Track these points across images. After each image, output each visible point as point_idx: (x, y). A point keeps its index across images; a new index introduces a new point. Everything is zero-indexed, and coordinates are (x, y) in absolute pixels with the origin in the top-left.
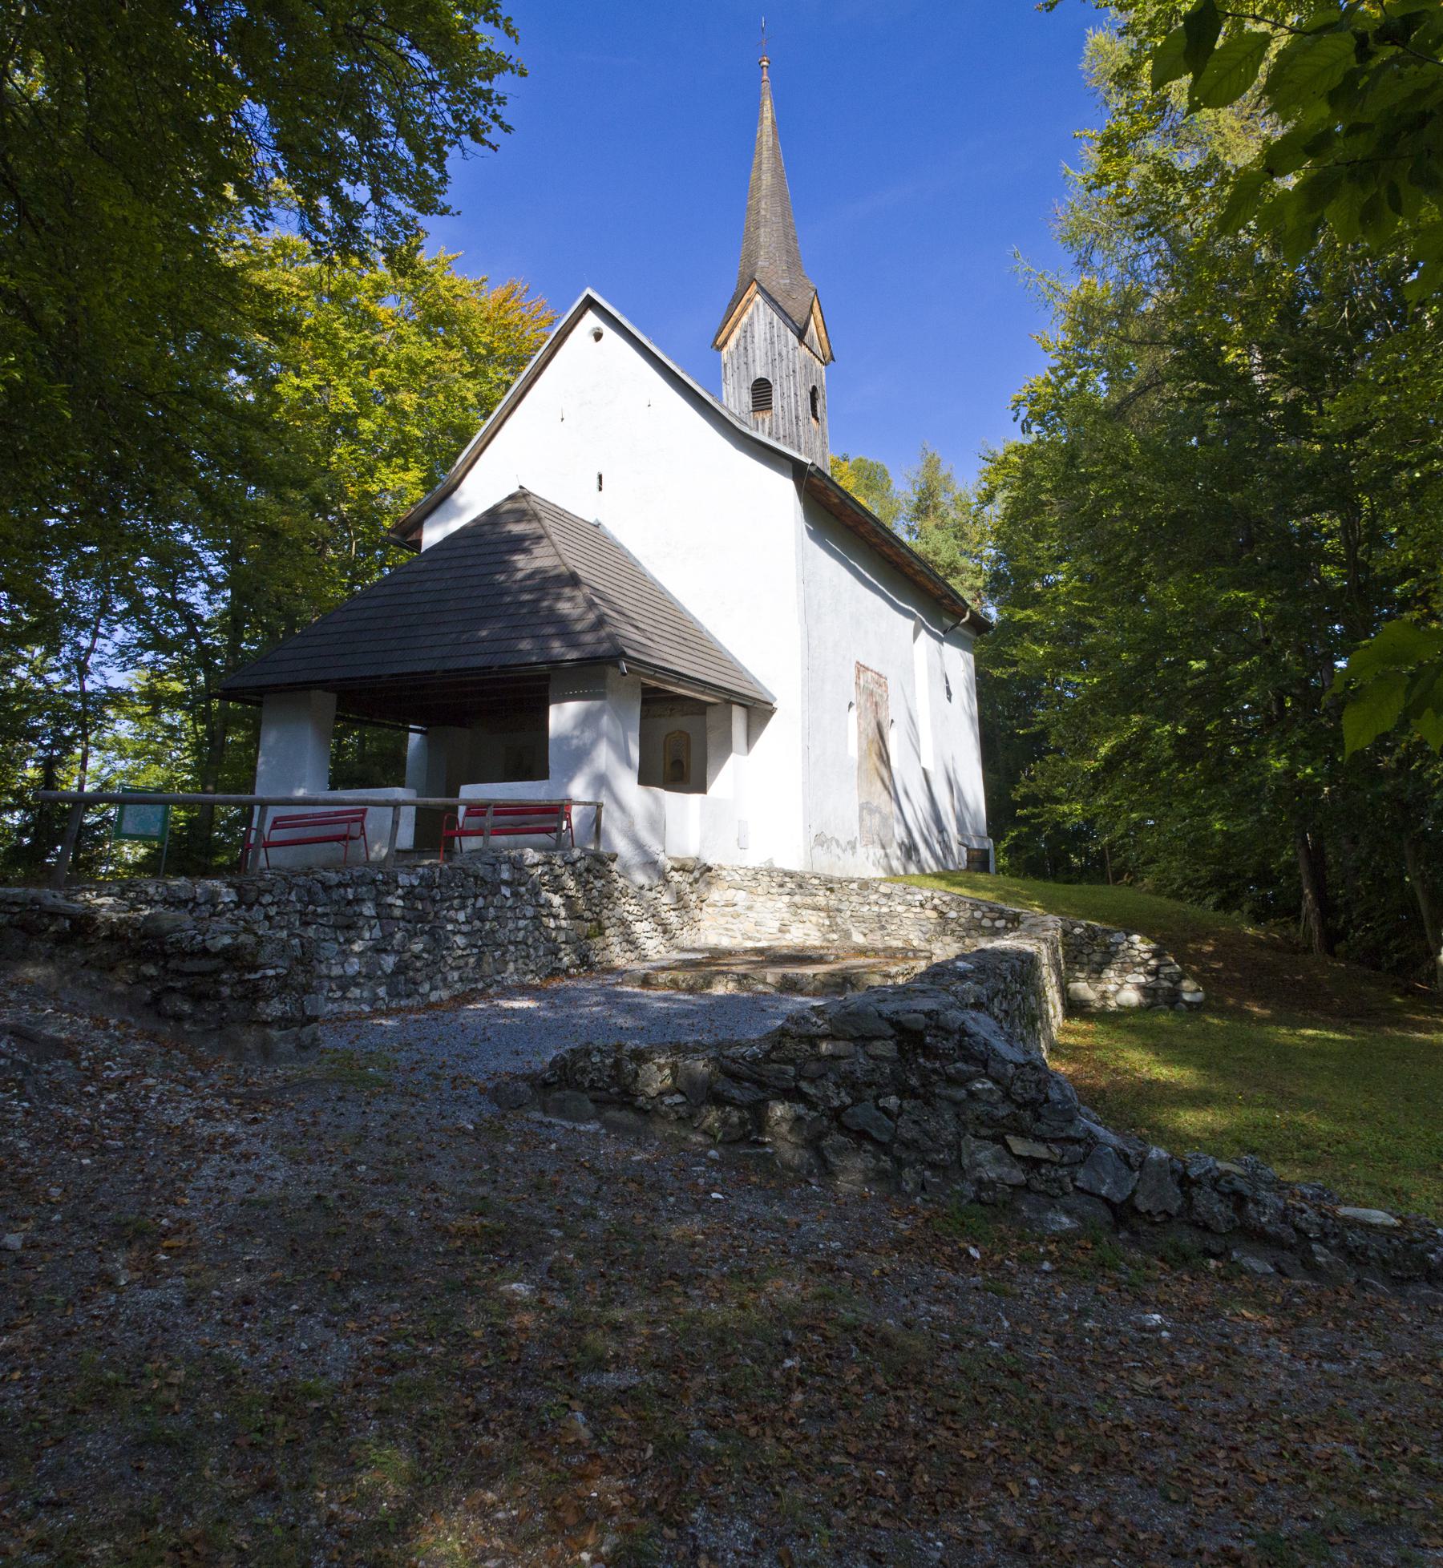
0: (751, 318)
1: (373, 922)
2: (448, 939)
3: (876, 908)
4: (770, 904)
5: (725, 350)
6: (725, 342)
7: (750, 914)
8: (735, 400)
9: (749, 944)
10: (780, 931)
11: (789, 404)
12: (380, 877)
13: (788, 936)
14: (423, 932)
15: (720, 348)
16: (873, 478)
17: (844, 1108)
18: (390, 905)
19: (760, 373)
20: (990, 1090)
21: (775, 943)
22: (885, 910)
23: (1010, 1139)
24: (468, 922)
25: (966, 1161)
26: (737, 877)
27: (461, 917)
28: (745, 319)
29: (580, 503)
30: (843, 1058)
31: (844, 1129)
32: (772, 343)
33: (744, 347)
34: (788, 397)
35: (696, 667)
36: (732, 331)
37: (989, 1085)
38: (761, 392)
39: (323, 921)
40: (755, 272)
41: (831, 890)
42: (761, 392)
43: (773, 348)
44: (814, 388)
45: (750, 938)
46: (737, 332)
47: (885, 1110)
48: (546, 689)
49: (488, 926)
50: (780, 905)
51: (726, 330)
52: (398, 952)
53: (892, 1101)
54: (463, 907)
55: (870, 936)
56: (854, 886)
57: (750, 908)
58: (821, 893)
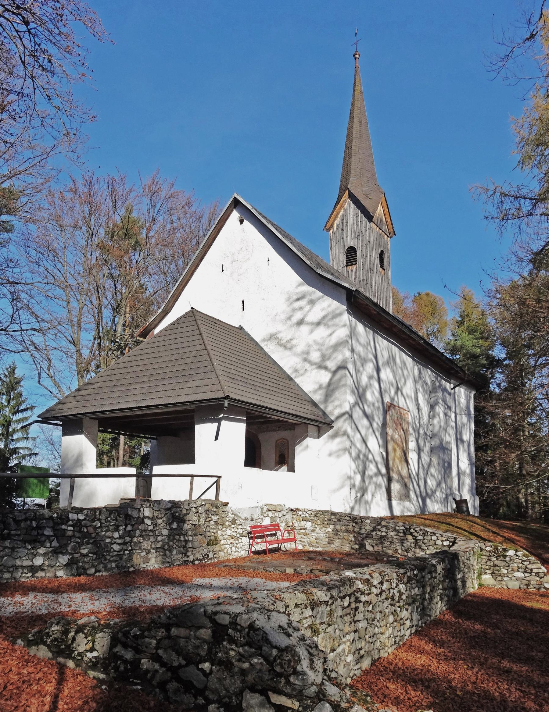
0: (346, 212)
1: (52, 538)
2: (107, 547)
3: (379, 533)
4: (323, 529)
5: (331, 231)
6: (331, 226)
7: (313, 534)
8: (336, 261)
9: (311, 549)
10: (329, 543)
11: (366, 261)
12: (55, 515)
13: (333, 546)
14: (88, 543)
15: (328, 230)
16: (433, 309)
17: (180, 666)
18: (65, 530)
19: (350, 243)
20: (261, 663)
21: (326, 549)
22: (384, 534)
23: (270, 693)
24: (120, 538)
25: (244, 704)
26: (307, 515)
27: (116, 535)
28: (342, 212)
29: (231, 317)
30: (181, 637)
31: (179, 679)
32: (357, 225)
33: (342, 228)
34: (367, 257)
35: (282, 404)
36: (335, 220)
37: (262, 660)
38: (351, 254)
39: (16, 538)
40: (347, 184)
41: (356, 523)
42: (351, 254)
43: (358, 229)
44: (382, 252)
45: (313, 546)
46: (338, 220)
47: (202, 670)
48: (193, 418)
49: (135, 540)
50: (329, 530)
51: (332, 219)
52: (70, 554)
53: (206, 666)
54: (117, 529)
55: (376, 547)
56: (368, 521)
57: (313, 531)
58: (351, 524)
